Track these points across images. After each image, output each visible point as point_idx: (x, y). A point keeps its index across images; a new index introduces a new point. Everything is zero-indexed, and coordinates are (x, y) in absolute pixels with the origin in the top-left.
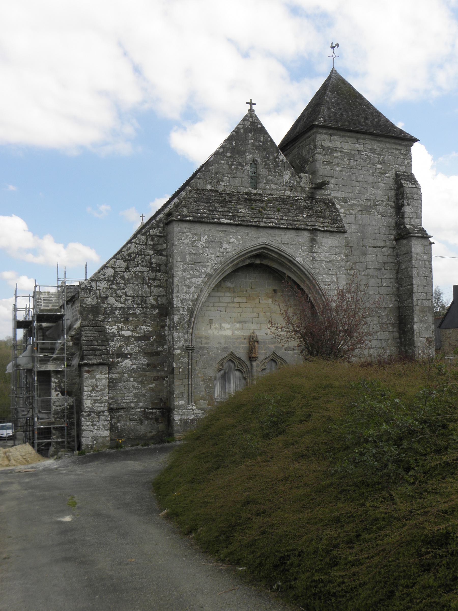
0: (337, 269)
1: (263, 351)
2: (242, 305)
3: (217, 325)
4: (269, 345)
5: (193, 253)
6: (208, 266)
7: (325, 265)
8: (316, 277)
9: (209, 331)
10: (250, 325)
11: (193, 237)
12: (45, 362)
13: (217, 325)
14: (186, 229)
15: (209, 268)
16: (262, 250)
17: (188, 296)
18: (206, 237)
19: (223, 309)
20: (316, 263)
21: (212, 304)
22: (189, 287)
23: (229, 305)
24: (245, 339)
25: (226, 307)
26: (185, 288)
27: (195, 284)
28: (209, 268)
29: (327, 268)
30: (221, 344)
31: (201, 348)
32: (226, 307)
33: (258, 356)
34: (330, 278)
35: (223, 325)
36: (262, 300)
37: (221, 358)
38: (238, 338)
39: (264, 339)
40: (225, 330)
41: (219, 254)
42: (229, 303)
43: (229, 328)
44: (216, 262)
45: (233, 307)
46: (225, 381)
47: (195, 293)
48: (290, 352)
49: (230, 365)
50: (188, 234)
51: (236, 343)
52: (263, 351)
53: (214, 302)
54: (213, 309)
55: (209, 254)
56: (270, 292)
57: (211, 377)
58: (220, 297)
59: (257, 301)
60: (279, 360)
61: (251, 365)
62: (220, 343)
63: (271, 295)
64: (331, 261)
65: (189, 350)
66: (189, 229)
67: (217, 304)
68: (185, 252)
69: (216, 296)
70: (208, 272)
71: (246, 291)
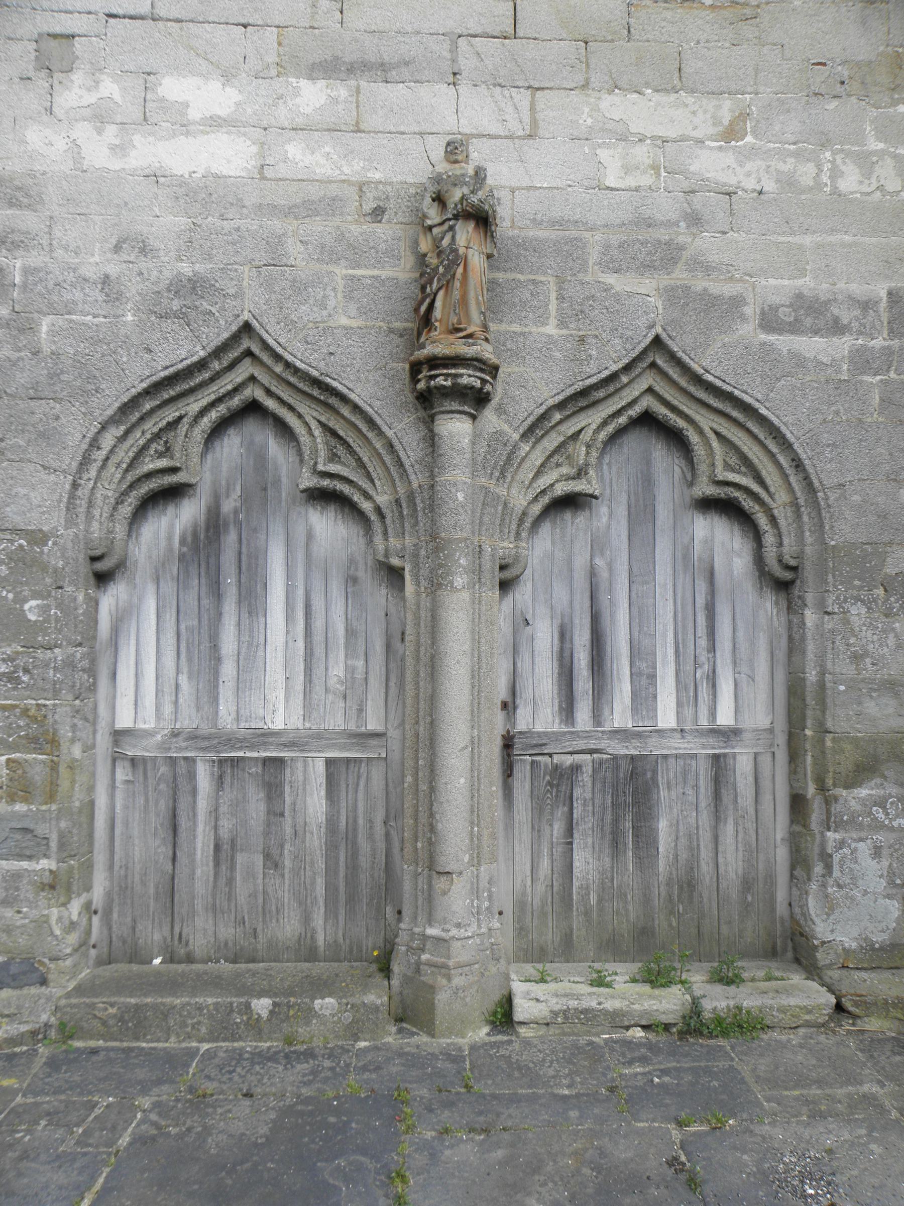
1: (551, 329)
3: (109, 88)
9: (35, 136)
12: (608, 829)
13: (109, 88)
16: (737, 494)
24: (378, 213)
30: (144, 250)
33: (486, 351)
39: (558, 223)
40: (185, 127)
43: (223, 112)
46: (216, 591)
49: (260, 459)
51: (294, 251)
52: (551, 329)
57: (38, 538)
60: (706, 421)
61: (432, 440)
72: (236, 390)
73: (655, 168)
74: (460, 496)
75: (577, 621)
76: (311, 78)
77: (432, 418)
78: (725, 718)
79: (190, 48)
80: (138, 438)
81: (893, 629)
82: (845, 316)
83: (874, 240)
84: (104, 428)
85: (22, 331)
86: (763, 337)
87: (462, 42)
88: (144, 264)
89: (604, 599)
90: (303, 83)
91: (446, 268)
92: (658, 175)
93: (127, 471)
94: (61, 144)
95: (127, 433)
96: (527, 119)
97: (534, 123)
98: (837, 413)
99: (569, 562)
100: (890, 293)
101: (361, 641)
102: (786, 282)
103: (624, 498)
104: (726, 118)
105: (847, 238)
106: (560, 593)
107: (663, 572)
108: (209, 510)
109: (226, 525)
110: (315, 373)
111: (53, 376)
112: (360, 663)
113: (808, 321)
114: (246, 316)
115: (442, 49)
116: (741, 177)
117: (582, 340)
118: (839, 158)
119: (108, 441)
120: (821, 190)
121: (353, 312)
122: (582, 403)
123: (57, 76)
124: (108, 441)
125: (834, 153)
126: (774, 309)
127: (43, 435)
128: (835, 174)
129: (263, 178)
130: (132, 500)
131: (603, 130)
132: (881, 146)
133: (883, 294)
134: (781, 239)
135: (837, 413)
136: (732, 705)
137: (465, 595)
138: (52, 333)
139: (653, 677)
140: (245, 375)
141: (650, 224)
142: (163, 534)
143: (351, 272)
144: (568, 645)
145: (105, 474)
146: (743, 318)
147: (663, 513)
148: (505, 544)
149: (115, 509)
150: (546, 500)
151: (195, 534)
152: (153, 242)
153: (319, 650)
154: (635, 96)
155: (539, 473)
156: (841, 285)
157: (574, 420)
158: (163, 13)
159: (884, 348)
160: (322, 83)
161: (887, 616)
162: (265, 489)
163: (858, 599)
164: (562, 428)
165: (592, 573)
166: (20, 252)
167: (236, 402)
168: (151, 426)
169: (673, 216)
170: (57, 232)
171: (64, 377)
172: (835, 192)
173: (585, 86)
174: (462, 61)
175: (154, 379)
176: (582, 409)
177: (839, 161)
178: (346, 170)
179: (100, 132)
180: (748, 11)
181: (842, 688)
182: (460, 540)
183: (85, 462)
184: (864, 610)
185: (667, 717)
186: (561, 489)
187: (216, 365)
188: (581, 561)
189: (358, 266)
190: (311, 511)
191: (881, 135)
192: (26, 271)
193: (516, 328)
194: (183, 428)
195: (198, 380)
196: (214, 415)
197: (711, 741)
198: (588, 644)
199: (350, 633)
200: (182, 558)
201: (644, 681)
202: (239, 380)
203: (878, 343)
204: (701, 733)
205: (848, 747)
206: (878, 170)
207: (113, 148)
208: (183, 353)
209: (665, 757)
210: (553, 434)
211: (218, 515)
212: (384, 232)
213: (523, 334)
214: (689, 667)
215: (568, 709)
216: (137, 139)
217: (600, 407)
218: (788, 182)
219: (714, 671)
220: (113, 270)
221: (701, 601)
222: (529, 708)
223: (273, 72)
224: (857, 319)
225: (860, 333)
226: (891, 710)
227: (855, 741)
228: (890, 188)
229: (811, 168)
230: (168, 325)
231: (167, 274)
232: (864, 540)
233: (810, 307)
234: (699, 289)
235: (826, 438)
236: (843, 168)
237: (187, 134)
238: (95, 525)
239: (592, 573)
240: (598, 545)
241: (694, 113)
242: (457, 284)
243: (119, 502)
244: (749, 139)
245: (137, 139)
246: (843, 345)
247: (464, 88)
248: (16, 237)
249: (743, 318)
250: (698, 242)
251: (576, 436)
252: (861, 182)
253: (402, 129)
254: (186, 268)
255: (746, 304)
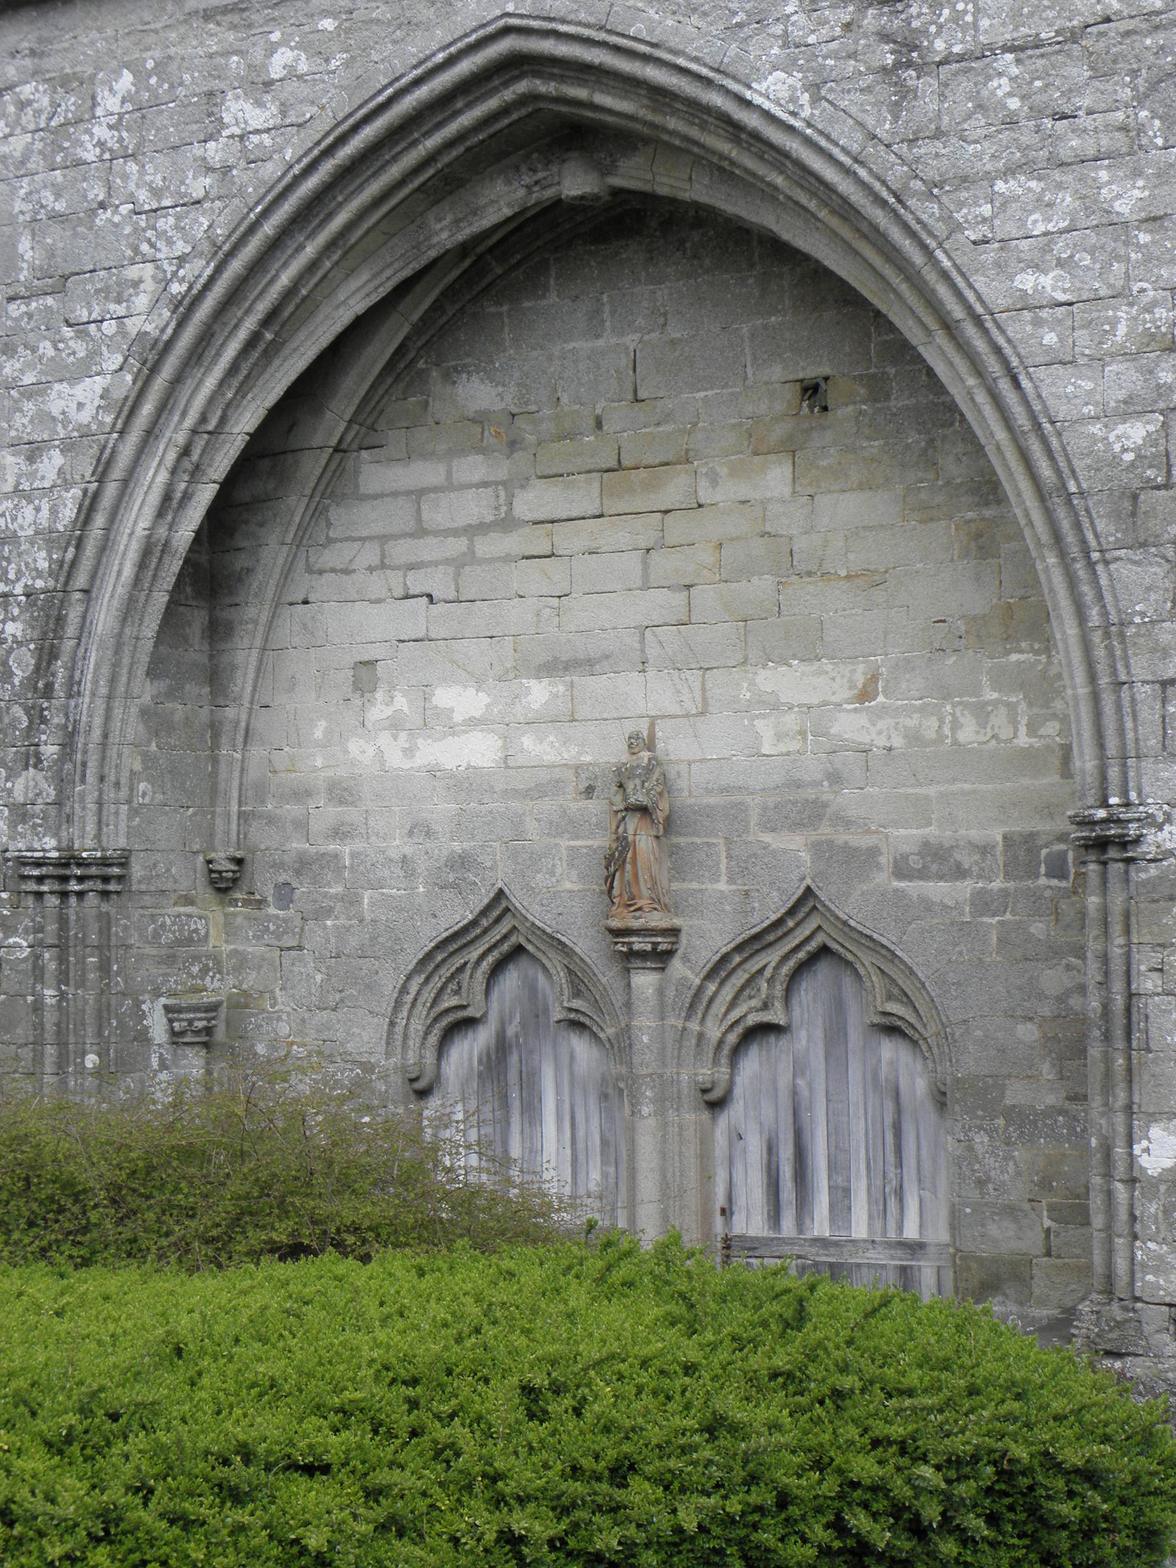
0: (1141, 99)
1: (722, 886)
2: (569, 539)
4: (773, 840)
5: (54, 216)
6: (136, 284)
7: (1020, 88)
8: (929, 211)
10: (629, 684)
11: (55, 105)
14: (18, 62)
15: (142, 301)
17: (28, 512)
18: (126, 80)
19: (438, 582)
20: (927, 85)
21: (369, 555)
22: (34, 451)
23: (487, 546)
24: (589, 791)
25: (458, 564)
26: (10, 460)
27: (66, 422)
28: (142, 301)
29: (1037, 112)
30: (429, 833)
31: (303, 864)
32: (458, 564)
34: (1067, 200)
35: (444, 697)
36: (714, 482)
37: (430, 933)
38: (540, 791)
39: (725, 790)
40: (452, 730)
41: (198, 186)
42: (481, 528)
44: (181, 247)
45: (507, 559)
47: (67, 485)
48: (937, 890)
50: (26, 91)
52: (722, 886)
53: (383, 539)
54: (376, 584)
55: (143, 195)
56: (779, 407)
58: (418, 494)
59: (674, 490)
62: (420, 829)
63: (780, 430)
64: (1074, 36)
65: (40, 879)
66: (33, 53)
67: (401, 551)
68: (12, 220)
69: (395, 494)
70: (134, 326)
71: (599, 424)
72: (505, 937)
73: (802, 733)
74: (645, 1039)
75: (781, 1136)
76: (538, 678)
77: (628, 970)
78: (911, 1232)
79: (454, 662)
80: (437, 982)
81: (1013, 1157)
82: (967, 860)
83: (990, 787)
84: (409, 978)
85: (351, 903)
86: (897, 884)
87: (648, 632)
88: (429, 845)
89: (805, 1115)
90: (533, 683)
91: (621, 853)
92: (805, 739)
93: (432, 1007)
94: (371, 751)
95: (427, 980)
96: (699, 699)
97: (705, 699)
98: (961, 953)
99: (774, 1082)
100: (1005, 838)
101: (612, 1149)
102: (914, 832)
103: (820, 1021)
104: (860, 680)
105: (967, 786)
106: (767, 1111)
107: (855, 1092)
108: (498, 1035)
109: (510, 1047)
110: (549, 930)
111: (374, 939)
112: (612, 1170)
113: (934, 867)
114: (500, 884)
115: (633, 641)
116: (874, 736)
117: (747, 894)
118: (958, 710)
119: (414, 988)
120: (942, 742)
121: (575, 878)
122: (757, 946)
123: (367, 695)
124: (414, 988)
125: (954, 706)
126: (905, 857)
127: (368, 986)
128: (956, 726)
129: (508, 767)
130: (437, 1031)
131: (759, 702)
132: (995, 695)
133: (999, 838)
134: (910, 791)
135: (961, 953)
136: (917, 1220)
137: (652, 1122)
138: (372, 904)
139: (847, 1191)
140: (509, 926)
141: (798, 785)
142: (465, 1056)
143: (572, 843)
144: (774, 1159)
145: (416, 1011)
146: (879, 867)
147: (855, 1036)
148: (704, 1071)
149: (425, 1038)
150: (739, 1030)
151: (488, 1055)
152: (436, 827)
153: (581, 1157)
154: (784, 668)
155: (732, 1005)
156: (962, 832)
157: (757, 958)
158: (433, 636)
159: (1001, 890)
160: (546, 681)
161: (1008, 1144)
162: (537, 1016)
163: (980, 1128)
164: (747, 966)
165: (794, 1093)
166: (348, 841)
167: (506, 947)
168: (445, 972)
169: (819, 776)
170: (371, 823)
171: (380, 940)
172: (955, 742)
173: (744, 663)
174: (648, 651)
175: (439, 939)
176: (758, 951)
177: (958, 714)
178: (566, 756)
179: (395, 738)
180: (877, 578)
181: (968, 1210)
182: (646, 1076)
183: (398, 1004)
184: (986, 1139)
185: (860, 1229)
186: (752, 1020)
187: (485, 923)
188: (784, 1081)
189: (577, 838)
190: (572, 1035)
191: (996, 686)
192: (353, 855)
193: (695, 885)
194: (468, 972)
195: (473, 935)
196: (490, 959)
197: (899, 1253)
198: (792, 1157)
199: (605, 1143)
200: (480, 1075)
201: (840, 1193)
202: (504, 931)
203: (997, 884)
204: (889, 1245)
205: (974, 1266)
206: (993, 720)
207: (404, 750)
208: (458, 918)
209: (859, 1265)
210: (740, 972)
211: (504, 1037)
212: (595, 807)
213: (700, 890)
214: (879, 1182)
215: (775, 1216)
216: (420, 741)
217: (777, 946)
218: (914, 738)
219: (901, 1187)
220: (408, 850)
221: (889, 1120)
222: (744, 1214)
223: (511, 676)
224: (977, 863)
225: (980, 877)
226: (1011, 1233)
227: (980, 1260)
228: (1003, 736)
229: (933, 722)
230: (448, 894)
231: (445, 853)
232: (986, 1072)
233: (935, 855)
234: (840, 842)
235: (952, 977)
236: (962, 720)
237: (454, 734)
238: (411, 1053)
239: (794, 1093)
240: (799, 1069)
241: (833, 679)
242: (628, 867)
243: (427, 1033)
244: (881, 699)
245: (420, 741)
246: (967, 887)
247: (651, 673)
248: (345, 829)
249: (879, 867)
250: (839, 799)
251: (761, 971)
252: (978, 733)
253: (605, 716)
254: (457, 846)
255: (881, 854)
